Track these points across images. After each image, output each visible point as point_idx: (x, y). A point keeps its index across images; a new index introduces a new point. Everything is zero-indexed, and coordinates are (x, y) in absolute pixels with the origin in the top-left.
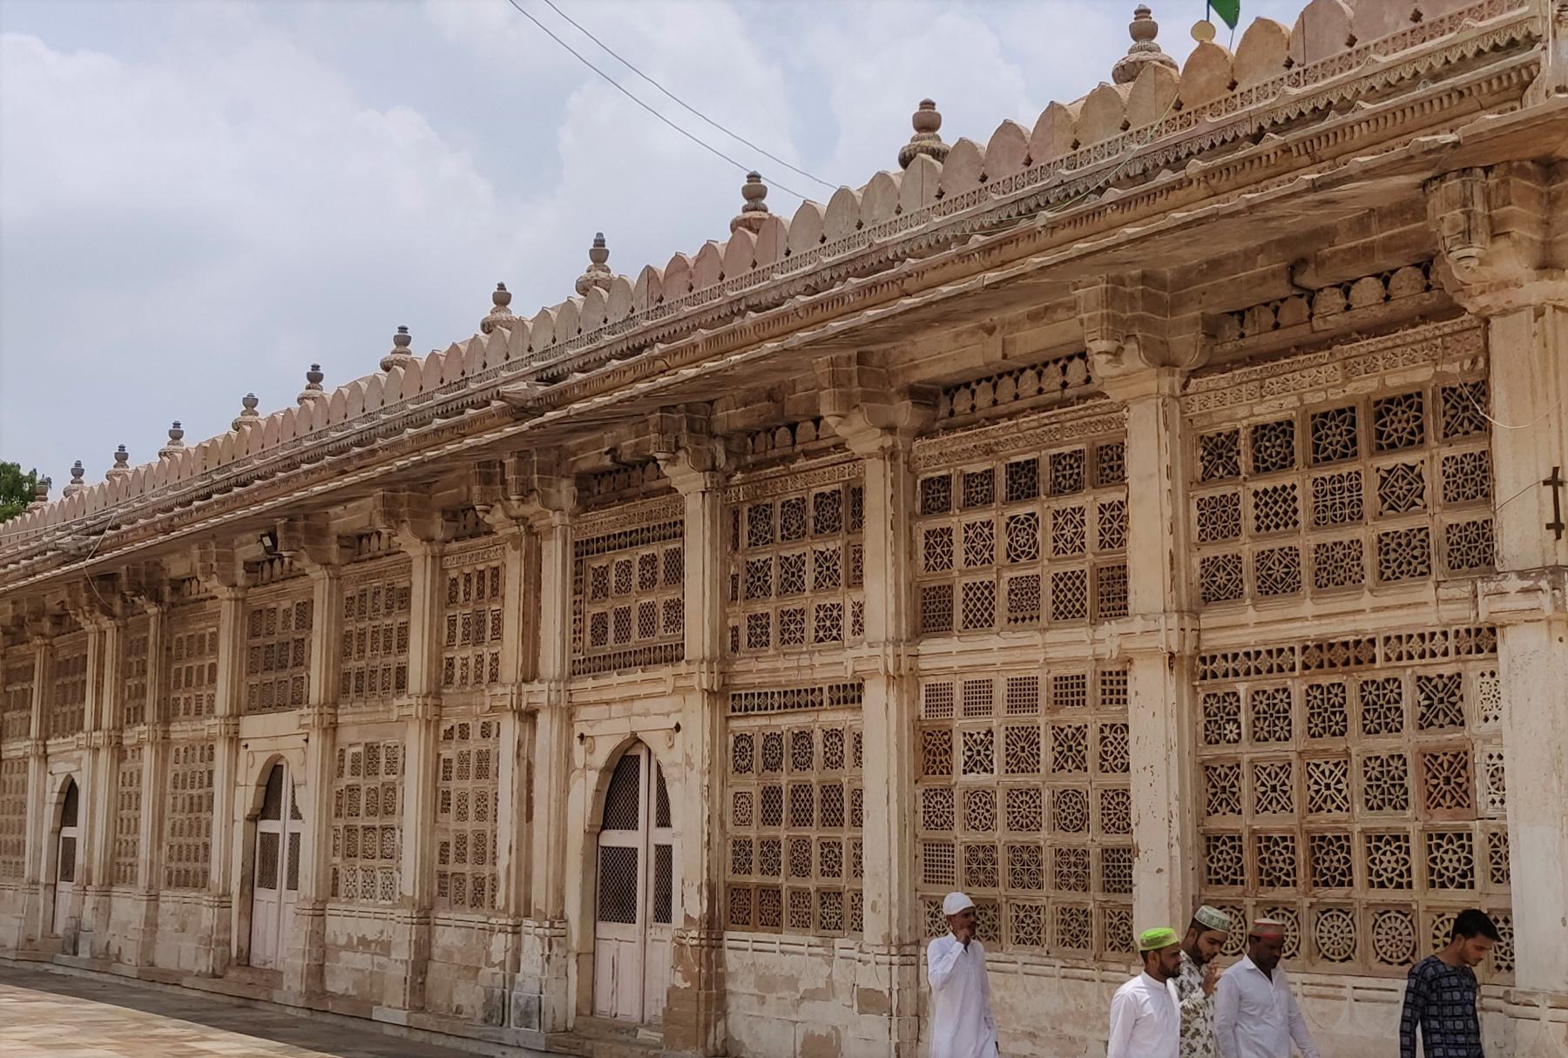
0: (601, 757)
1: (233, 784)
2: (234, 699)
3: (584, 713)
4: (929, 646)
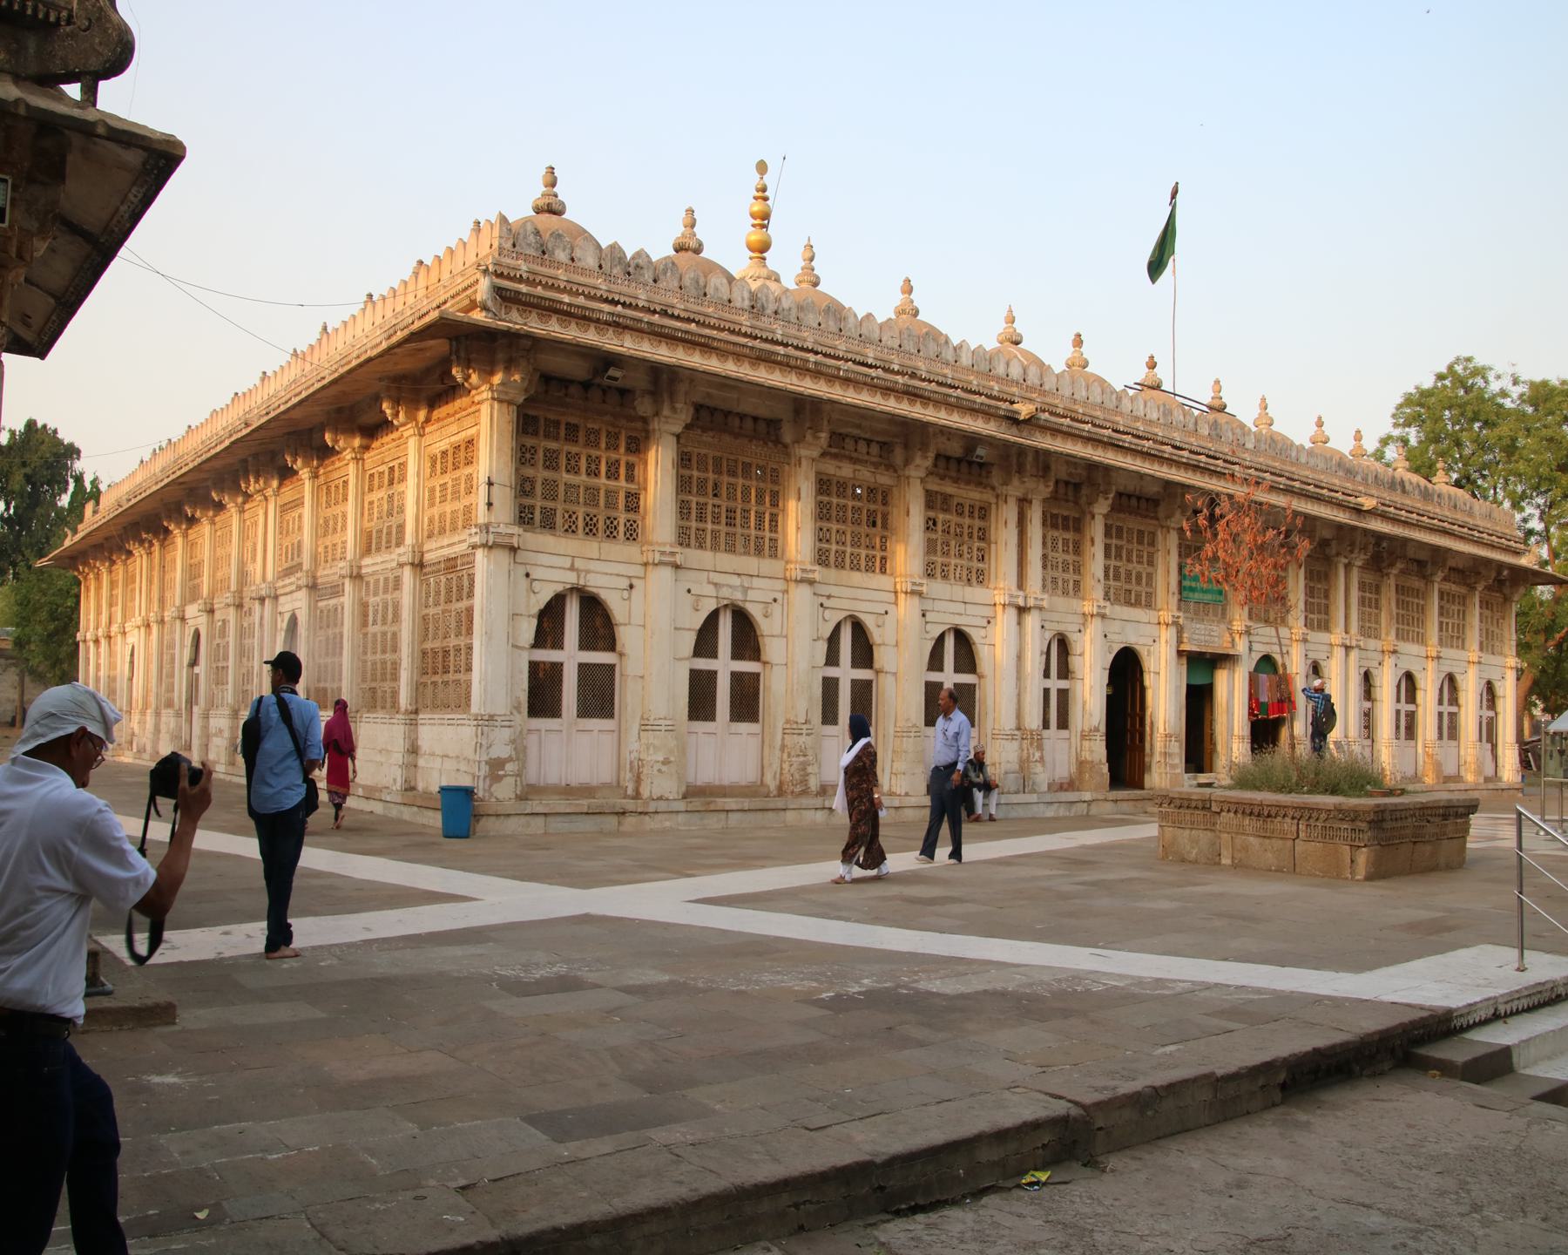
0: (285, 625)
1: (182, 646)
2: (183, 598)
3: (282, 600)
4: (367, 561)
